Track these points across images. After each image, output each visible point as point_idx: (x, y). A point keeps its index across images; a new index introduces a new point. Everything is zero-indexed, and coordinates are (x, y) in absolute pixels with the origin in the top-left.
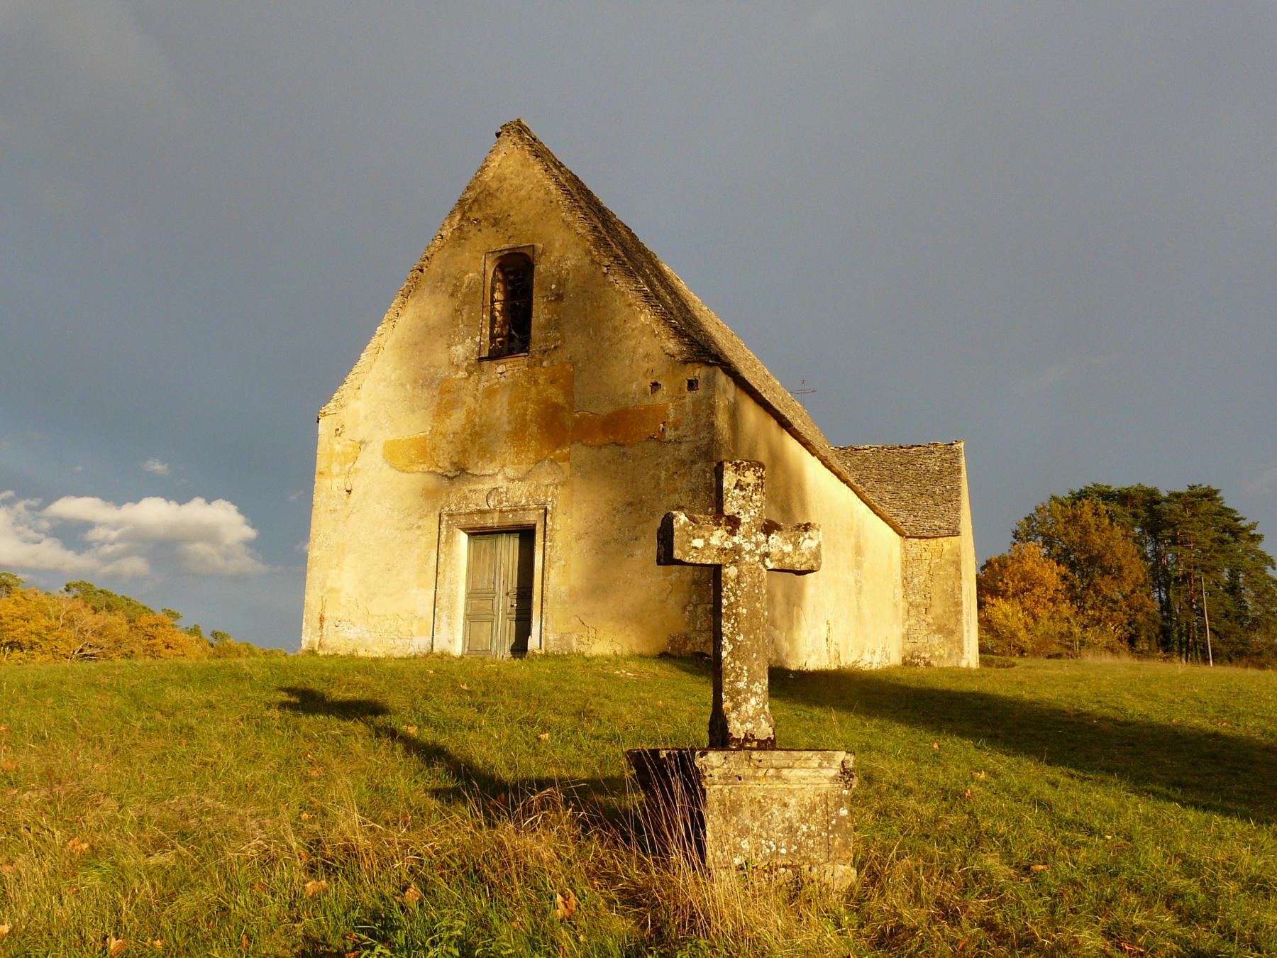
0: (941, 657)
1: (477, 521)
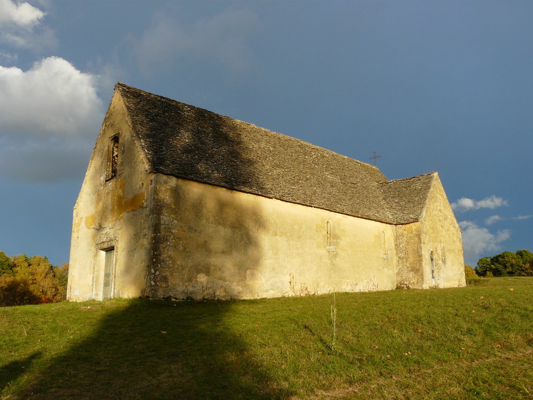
0: (414, 283)
1: (105, 246)
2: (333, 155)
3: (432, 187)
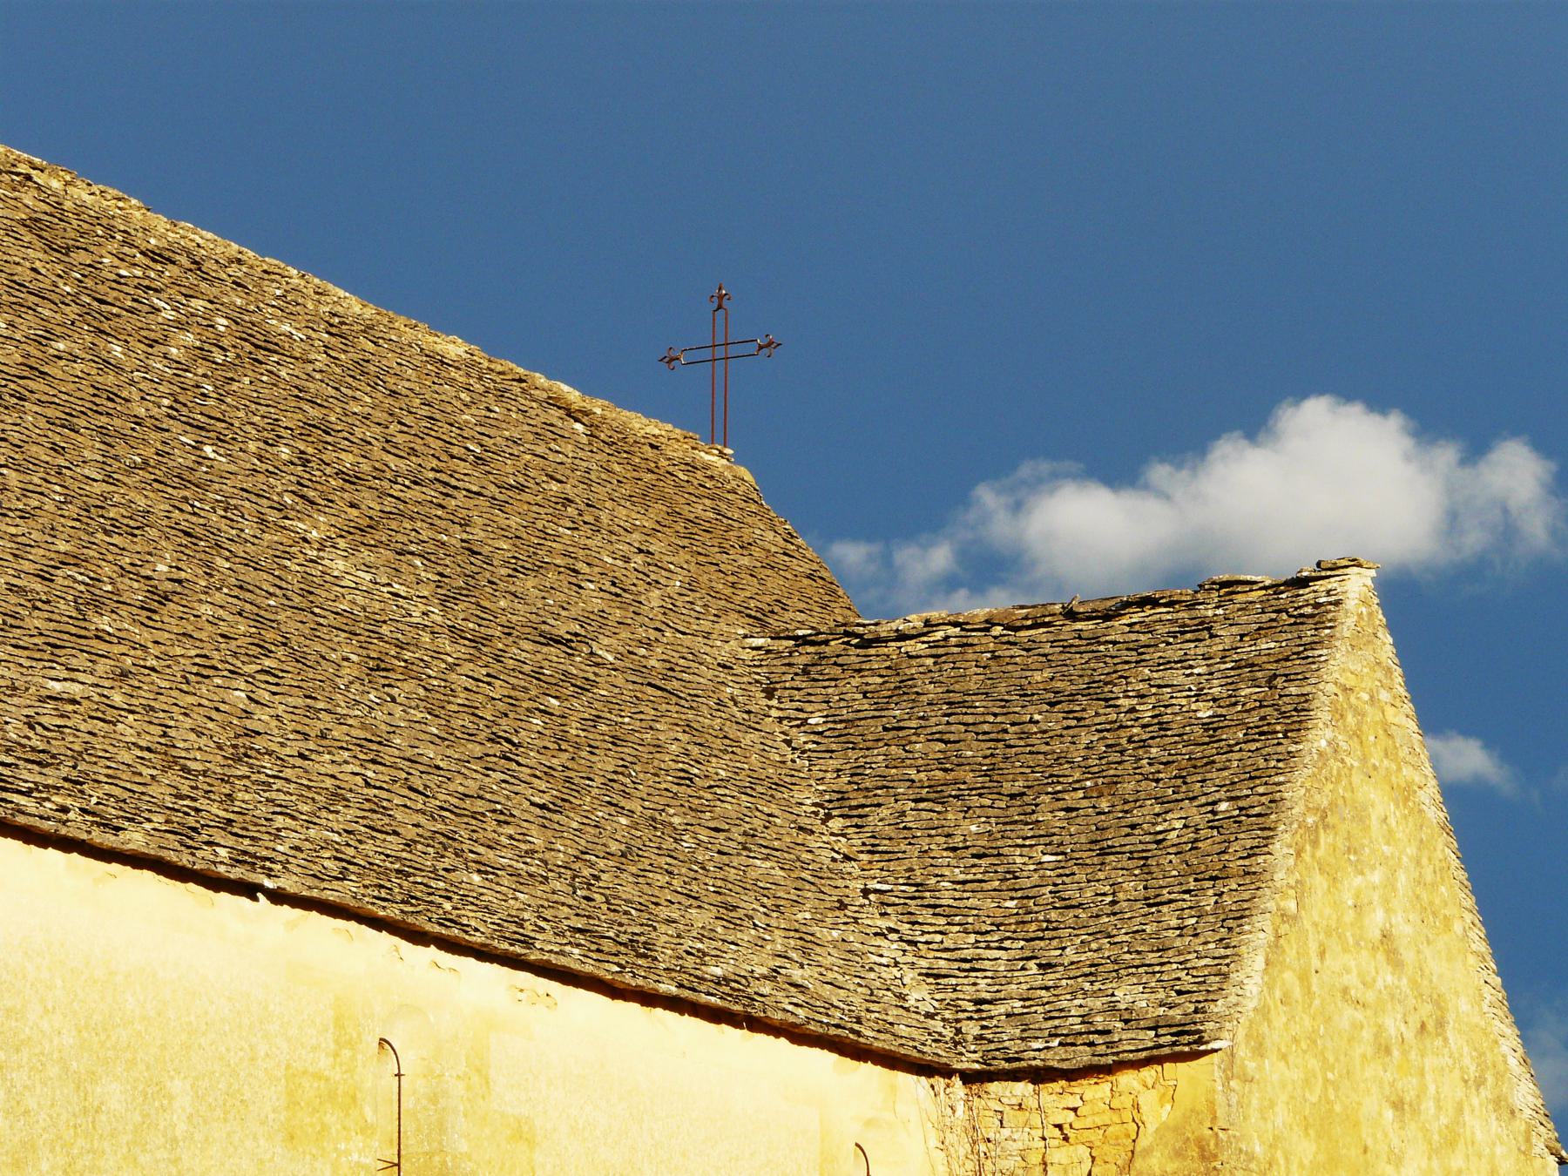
2: (337, 327)
3: (1321, 714)
